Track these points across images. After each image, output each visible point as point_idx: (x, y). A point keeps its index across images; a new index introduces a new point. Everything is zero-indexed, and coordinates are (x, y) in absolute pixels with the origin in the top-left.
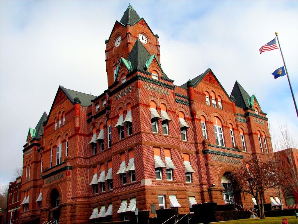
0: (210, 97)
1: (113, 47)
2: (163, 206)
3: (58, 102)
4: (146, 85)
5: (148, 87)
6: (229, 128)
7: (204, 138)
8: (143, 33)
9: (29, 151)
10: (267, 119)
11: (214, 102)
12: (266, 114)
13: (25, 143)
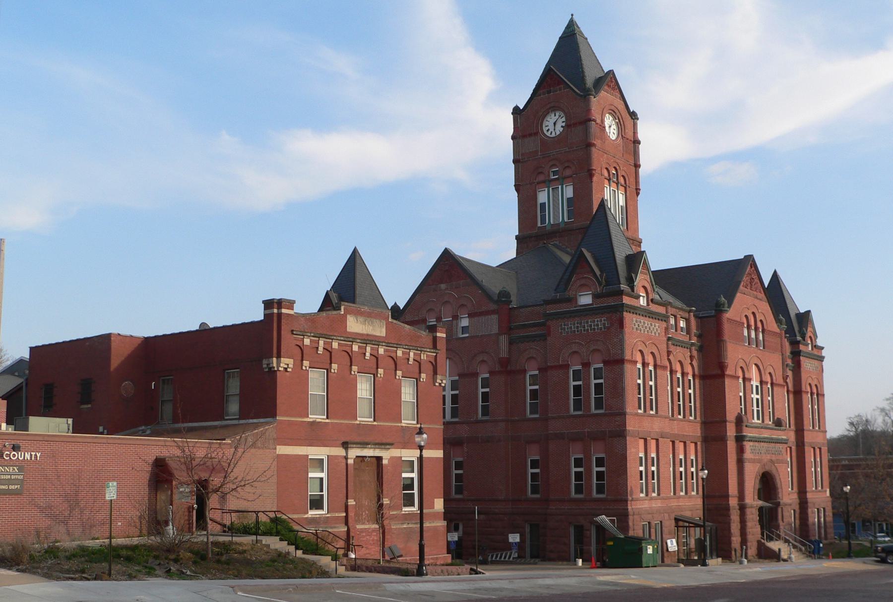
0: (749, 327)
6: (636, 362)
8: (614, 113)
10: (824, 357)
12: (822, 348)
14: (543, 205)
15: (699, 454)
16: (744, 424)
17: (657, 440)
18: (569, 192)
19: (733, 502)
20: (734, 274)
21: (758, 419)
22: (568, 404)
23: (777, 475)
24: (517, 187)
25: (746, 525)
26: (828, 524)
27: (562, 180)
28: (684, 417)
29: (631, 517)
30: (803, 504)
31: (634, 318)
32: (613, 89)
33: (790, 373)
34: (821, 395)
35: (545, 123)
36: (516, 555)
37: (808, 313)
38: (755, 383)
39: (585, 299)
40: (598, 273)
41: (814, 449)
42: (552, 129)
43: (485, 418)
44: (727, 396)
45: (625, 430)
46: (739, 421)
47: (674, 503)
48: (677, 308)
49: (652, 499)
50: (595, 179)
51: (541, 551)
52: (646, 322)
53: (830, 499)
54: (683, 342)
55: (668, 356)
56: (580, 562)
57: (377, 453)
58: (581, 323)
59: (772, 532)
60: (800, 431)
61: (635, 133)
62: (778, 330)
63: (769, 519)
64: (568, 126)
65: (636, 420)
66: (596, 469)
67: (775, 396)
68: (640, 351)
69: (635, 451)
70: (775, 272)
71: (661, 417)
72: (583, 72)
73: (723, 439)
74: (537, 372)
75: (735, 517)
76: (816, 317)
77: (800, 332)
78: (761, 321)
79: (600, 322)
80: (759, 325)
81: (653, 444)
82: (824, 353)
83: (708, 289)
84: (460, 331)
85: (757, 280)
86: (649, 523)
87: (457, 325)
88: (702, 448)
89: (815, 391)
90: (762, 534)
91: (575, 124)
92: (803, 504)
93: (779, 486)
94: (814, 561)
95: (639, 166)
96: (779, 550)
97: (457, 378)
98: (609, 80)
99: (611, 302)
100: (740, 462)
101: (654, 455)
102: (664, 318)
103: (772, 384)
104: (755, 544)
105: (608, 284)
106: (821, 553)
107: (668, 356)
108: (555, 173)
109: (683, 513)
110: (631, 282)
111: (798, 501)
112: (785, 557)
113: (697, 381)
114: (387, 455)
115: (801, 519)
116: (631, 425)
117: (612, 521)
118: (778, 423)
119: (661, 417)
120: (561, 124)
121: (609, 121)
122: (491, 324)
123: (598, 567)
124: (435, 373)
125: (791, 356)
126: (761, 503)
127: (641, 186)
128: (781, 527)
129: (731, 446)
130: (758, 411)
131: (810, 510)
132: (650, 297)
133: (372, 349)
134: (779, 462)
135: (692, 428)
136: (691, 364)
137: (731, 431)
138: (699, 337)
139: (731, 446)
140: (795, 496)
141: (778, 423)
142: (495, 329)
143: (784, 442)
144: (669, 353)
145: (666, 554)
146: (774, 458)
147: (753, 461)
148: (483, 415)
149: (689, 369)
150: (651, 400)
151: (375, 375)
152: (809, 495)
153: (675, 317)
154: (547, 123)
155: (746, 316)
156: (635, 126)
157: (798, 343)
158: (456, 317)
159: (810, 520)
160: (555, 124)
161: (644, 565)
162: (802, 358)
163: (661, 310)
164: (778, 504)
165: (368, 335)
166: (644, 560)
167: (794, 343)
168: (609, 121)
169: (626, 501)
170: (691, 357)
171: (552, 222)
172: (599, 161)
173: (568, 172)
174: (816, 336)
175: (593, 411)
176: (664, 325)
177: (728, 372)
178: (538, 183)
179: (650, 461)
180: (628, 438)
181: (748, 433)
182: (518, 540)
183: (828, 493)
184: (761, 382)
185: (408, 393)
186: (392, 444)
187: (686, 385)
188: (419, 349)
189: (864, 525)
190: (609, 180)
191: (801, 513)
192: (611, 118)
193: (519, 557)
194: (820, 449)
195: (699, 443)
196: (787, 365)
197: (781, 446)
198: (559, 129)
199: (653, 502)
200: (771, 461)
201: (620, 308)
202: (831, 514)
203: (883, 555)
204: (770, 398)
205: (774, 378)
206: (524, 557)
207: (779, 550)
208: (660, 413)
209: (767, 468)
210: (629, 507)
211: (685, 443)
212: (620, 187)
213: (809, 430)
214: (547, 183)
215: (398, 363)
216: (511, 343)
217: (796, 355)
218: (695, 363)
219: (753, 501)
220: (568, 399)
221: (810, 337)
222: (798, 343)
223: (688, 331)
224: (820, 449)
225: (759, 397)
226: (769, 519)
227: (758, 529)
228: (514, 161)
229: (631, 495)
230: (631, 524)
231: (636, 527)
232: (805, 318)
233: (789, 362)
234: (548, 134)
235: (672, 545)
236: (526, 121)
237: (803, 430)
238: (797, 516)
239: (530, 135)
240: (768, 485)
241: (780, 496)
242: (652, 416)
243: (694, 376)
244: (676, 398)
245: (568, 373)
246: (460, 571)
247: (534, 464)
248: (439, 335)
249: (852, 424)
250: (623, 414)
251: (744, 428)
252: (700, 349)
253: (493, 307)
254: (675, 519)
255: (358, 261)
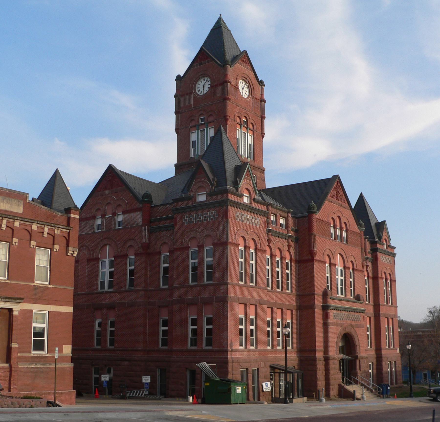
0: (335, 227)
2: (44, 328)
6: (238, 245)
7: (326, 288)
8: (246, 80)
10: (395, 254)
11: (338, 232)
12: (395, 248)
14: (194, 142)
15: (294, 319)
16: (329, 297)
17: (256, 306)
18: (211, 132)
19: (320, 355)
20: (326, 188)
21: (342, 294)
22: (187, 276)
23: (355, 336)
24: (177, 130)
25: (329, 373)
26: (398, 373)
27: (207, 124)
28: (282, 290)
29: (230, 365)
30: (379, 358)
31: (238, 212)
32: (246, 63)
33: (370, 264)
34: (393, 281)
35: (197, 86)
36: (147, 393)
37: (384, 222)
38: (339, 268)
39: (202, 198)
40: (211, 176)
41: (388, 318)
42: (201, 90)
43: (132, 288)
44: (315, 275)
45: (227, 296)
46: (325, 295)
47: (270, 355)
48: (277, 209)
49: (250, 351)
50: (229, 123)
51: (165, 390)
52: (248, 216)
53: (400, 355)
54: (281, 234)
55: (269, 243)
56: (191, 399)
57: (8, 305)
58: (198, 216)
59: (350, 378)
60: (377, 306)
61: (262, 95)
62: (358, 231)
63: (349, 369)
64: (212, 87)
65: (236, 289)
66: (206, 327)
67: (355, 278)
68: (243, 237)
69: (236, 313)
70: (361, 194)
71: (260, 288)
72: (224, 50)
73: (312, 308)
74: (168, 254)
75: (320, 366)
76: (389, 226)
77: (377, 235)
78: (345, 223)
79: (211, 214)
80: (343, 225)
81: (252, 308)
82: (396, 251)
83: (305, 201)
84: (117, 225)
85: (341, 193)
86: (247, 369)
87: (115, 220)
88: (297, 315)
89: (388, 277)
90: (343, 380)
91: (216, 85)
92: (379, 358)
93: (357, 344)
94: (382, 400)
95: (264, 118)
96: (354, 391)
97: (113, 259)
98: (244, 57)
99: (220, 198)
100: (326, 325)
101: (253, 317)
102: (266, 215)
103: (353, 269)
104: (337, 387)
105: (218, 185)
106: (389, 394)
107: (269, 243)
108: (202, 120)
109: (278, 363)
110: (236, 184)
111: (375, 356)
112: (359, 397)
113: (293, 264)
114: (17, 308)
115: (377, 369)
116: (232, 293)
117: (213, 368)
118: (357, 298)
119: (260, 288)
120: (207, 86)
121: (241, 84)
122: (138, 218)
123: (199, 403)
124: (68, 245)
125: (371, 252)
126: (342, 356)
127: (266, 132)
128: (359, 375)
129: (318, 313)
130: (342, 289)
131: (384, 363)
132: (253, 197)
133: (8, 222)
134: (357, 326)
135: (289, 298)
136: (289, 251)
137: (318, 302)
138: (296, 231)
139: (318, 313)
140: (372, 353)
141: (357, 298)
142: (140, 222)
143: (363, 312)
144: (269, 241)
145: (261, 394)
146: (353, 323)
147: (336, 325)
148: (130, 286)
149: (287, 255)
150: (252, 275)
151: (11, 243)
152: (383, 352)
153: (276, 215)
154: (199, 86)
155: (333, 218)
156: (262, 90)
157: (376, 242)
158: (114, 214)
159: (384, 370)
160: (204, 86)
161: (233, 402)
162: (378, 254)
163: (263, 208)
164: (356, 357)
165: (5, 211)
166: (232, 398)
167: (373, 243)
168: (241, 84)
169: (227, 351)
170: (289, 246)
171: (199, 154)
172: (232, 110)
173: (211, 119)
174: (390, 239)
175: (205, 282)
176: (265, 219)
177: (316, 258)
178: (191, 127)
179: (249, 322)
180: (229, 302)
181: (331, 303)
182: (149, 381)
183: (398, 351)
184: (345, 267)
185: (42, 259)
186: (22, 299)
187: (285, 266)
188: (53, 225)
189: (432, 375)
190: (241, 125)
191: (377, 365)
192: (244, 83)
193: (150, 394)
194: (392, 319)
195: (294, 311)
196: (367, 258)
197: (359, 315)
198: (206, 89)
199: (251, 353)
200: (352, 326)
201: (225, 203)
202: (400, 366)
203: (434, 395)
204: (351, 280)
205: (355, 265)
206: (156, 394)
207: (354, 391)
208: (259, 285)
209: (347, 330)
210: (229, 357)
211: (282, 310)
212: (242, 127)
213: (384, 305)
214: (197, 126)
215: (32, 235)
216: (151, 232)
217: (374, 251)
218: (292, 250)
219: (335, 354)
220: (188, 273)
221: (385, 239)
222: (376, 242)
223: (287, 227)
224: (392, 319)
225: (343, 278)
226: (349, 369)
227: (340, 376)
228: (176, 113)
229: (231, 347)
230: (230, 369)
231: (234, 372)
232: (381, 226)
233: (369, 256)
234: (199, 93)
235: (267, 386)
236: (185, 83)
237: (379, 305)
238: (375, 366)
239: (187, 94)
240: (348, 342)
241: (358, 351)
242: (252, 287)
243: (291, 260)
244: (275, 275)
245: (188, 254)
246: (33, 403)
247: (165, 323)
248: (72, 216)
249: (430, 312)
250: (226, 284)
251: (329, 300)
252: (297, 241)
253: (139, 206)
254: (270, 367)
255: (58, 178)
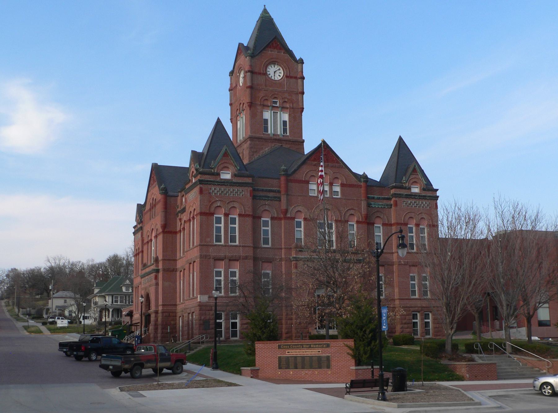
1: (237, 85)
3: (152, 185)
4: (211, 189)
5: (213, 191)
9: (137, 235)
13: (135, 224)
